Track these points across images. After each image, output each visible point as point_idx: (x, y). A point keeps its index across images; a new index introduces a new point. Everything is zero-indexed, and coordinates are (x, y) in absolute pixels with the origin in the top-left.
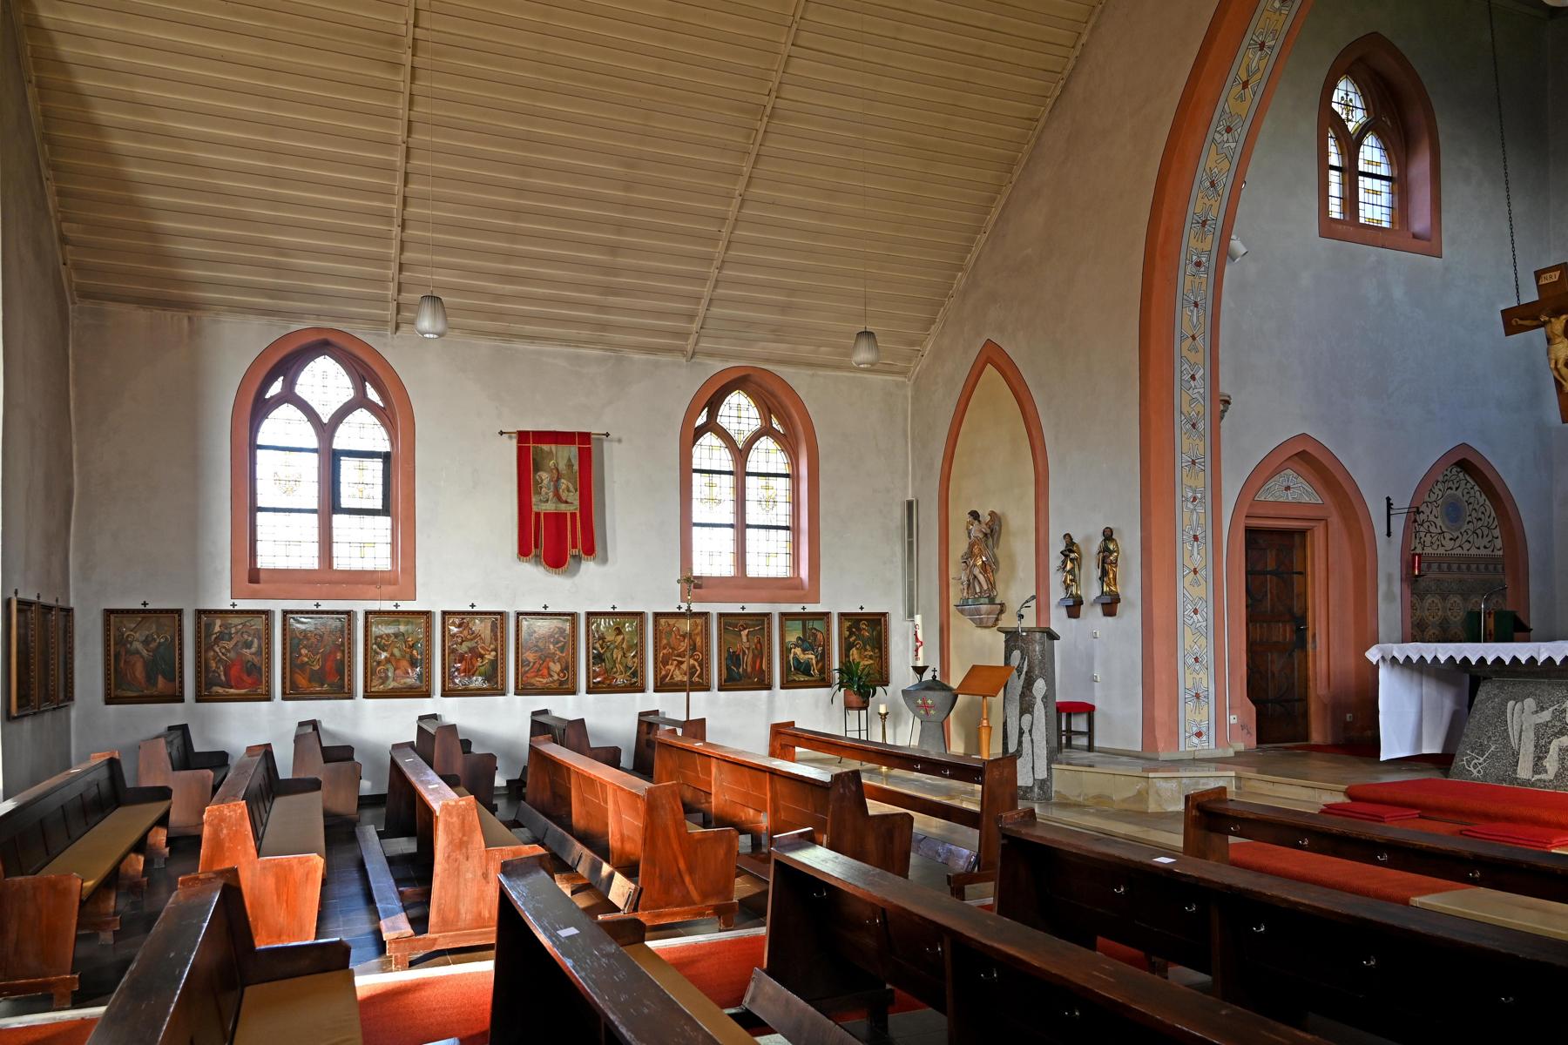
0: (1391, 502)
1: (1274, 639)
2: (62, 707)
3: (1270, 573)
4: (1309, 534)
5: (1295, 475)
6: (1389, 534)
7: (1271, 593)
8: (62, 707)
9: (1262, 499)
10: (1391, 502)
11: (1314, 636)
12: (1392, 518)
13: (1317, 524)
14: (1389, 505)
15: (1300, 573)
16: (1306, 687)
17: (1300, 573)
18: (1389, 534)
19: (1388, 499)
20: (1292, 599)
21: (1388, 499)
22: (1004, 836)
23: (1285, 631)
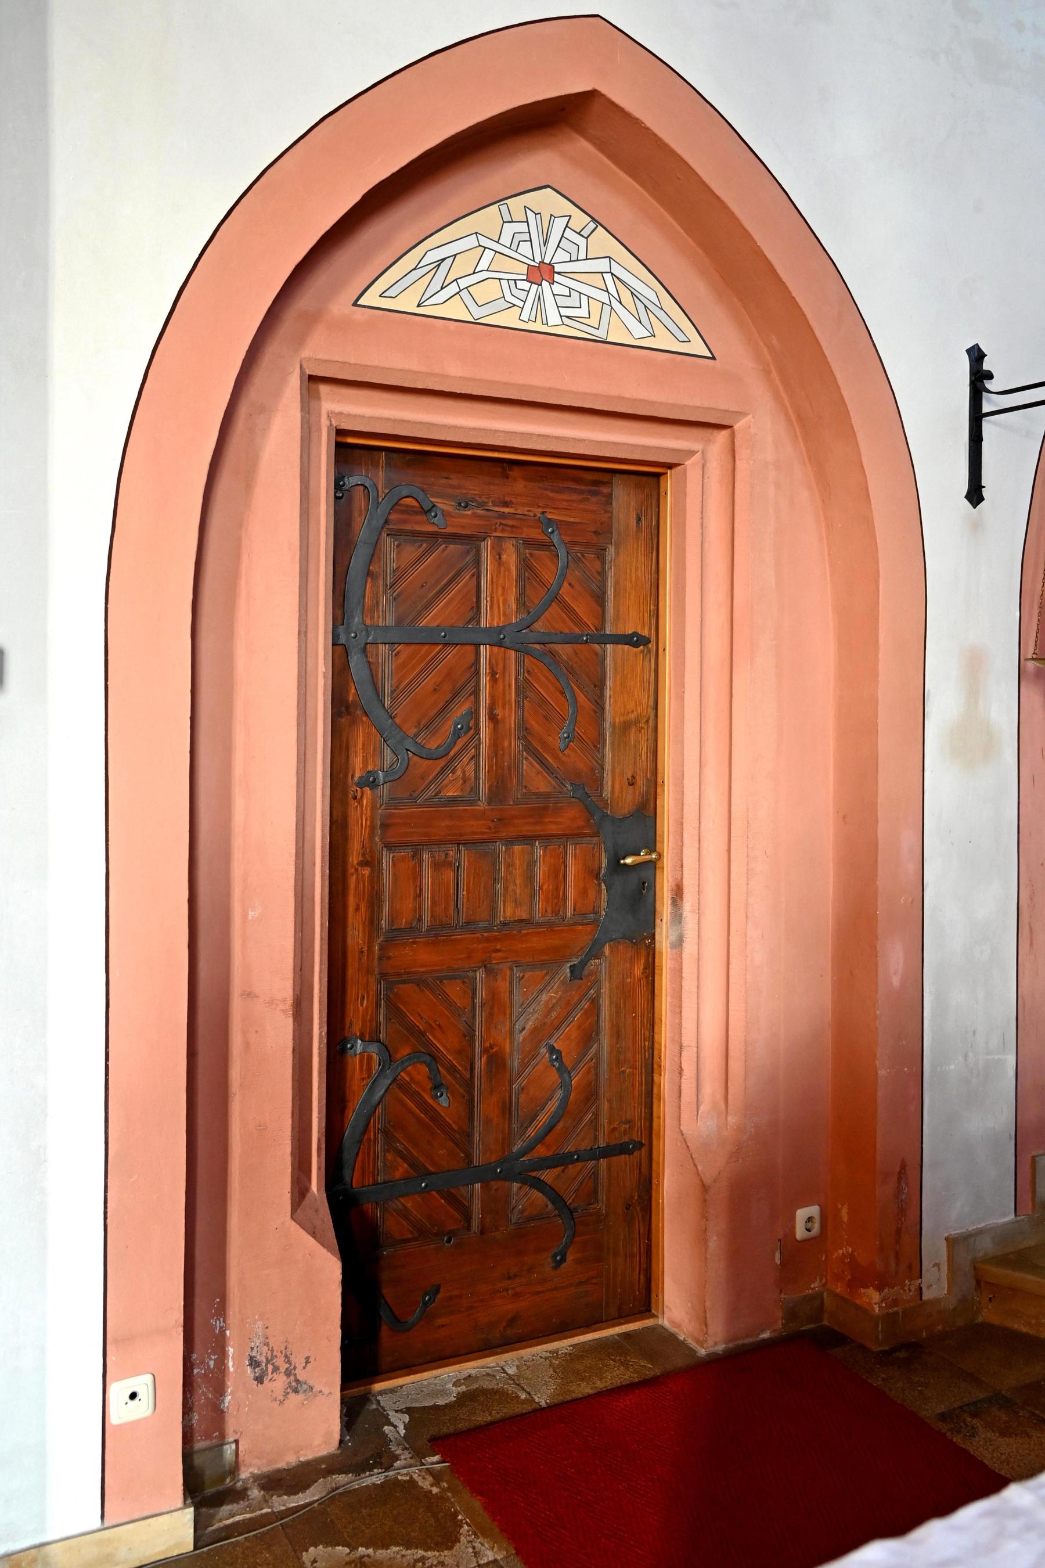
0: (986, 366)
1: (507, 911)
2: (407, 1055)
3: (497, 639)
4: (669, 483)
5: (580, 220)
6: (975, 494)
7: (492, 717)
8: (407, 1055)
9: (407, 303)
10: (986, 366)
11: (678, 892)
12: (988, 426)
13: (697, 446)
14: (979, 378)
15: (636, 640)
16: (649, 1095)
17: (636, 640)
18: (975, 494)
19: (976, 355)
20: (598, 741)
21: (976, 355)
22: (338, 1449)
23: (558, 874)
